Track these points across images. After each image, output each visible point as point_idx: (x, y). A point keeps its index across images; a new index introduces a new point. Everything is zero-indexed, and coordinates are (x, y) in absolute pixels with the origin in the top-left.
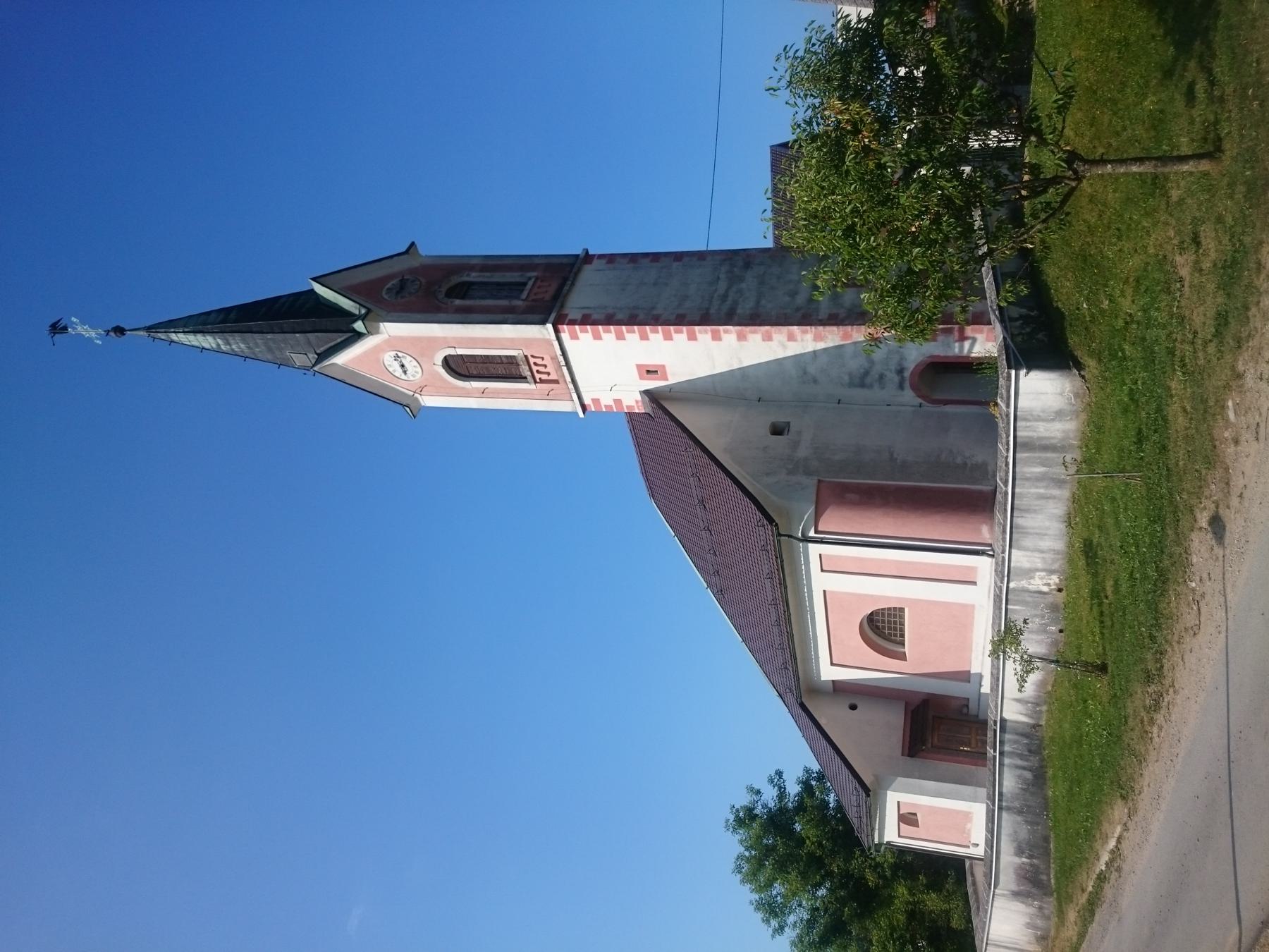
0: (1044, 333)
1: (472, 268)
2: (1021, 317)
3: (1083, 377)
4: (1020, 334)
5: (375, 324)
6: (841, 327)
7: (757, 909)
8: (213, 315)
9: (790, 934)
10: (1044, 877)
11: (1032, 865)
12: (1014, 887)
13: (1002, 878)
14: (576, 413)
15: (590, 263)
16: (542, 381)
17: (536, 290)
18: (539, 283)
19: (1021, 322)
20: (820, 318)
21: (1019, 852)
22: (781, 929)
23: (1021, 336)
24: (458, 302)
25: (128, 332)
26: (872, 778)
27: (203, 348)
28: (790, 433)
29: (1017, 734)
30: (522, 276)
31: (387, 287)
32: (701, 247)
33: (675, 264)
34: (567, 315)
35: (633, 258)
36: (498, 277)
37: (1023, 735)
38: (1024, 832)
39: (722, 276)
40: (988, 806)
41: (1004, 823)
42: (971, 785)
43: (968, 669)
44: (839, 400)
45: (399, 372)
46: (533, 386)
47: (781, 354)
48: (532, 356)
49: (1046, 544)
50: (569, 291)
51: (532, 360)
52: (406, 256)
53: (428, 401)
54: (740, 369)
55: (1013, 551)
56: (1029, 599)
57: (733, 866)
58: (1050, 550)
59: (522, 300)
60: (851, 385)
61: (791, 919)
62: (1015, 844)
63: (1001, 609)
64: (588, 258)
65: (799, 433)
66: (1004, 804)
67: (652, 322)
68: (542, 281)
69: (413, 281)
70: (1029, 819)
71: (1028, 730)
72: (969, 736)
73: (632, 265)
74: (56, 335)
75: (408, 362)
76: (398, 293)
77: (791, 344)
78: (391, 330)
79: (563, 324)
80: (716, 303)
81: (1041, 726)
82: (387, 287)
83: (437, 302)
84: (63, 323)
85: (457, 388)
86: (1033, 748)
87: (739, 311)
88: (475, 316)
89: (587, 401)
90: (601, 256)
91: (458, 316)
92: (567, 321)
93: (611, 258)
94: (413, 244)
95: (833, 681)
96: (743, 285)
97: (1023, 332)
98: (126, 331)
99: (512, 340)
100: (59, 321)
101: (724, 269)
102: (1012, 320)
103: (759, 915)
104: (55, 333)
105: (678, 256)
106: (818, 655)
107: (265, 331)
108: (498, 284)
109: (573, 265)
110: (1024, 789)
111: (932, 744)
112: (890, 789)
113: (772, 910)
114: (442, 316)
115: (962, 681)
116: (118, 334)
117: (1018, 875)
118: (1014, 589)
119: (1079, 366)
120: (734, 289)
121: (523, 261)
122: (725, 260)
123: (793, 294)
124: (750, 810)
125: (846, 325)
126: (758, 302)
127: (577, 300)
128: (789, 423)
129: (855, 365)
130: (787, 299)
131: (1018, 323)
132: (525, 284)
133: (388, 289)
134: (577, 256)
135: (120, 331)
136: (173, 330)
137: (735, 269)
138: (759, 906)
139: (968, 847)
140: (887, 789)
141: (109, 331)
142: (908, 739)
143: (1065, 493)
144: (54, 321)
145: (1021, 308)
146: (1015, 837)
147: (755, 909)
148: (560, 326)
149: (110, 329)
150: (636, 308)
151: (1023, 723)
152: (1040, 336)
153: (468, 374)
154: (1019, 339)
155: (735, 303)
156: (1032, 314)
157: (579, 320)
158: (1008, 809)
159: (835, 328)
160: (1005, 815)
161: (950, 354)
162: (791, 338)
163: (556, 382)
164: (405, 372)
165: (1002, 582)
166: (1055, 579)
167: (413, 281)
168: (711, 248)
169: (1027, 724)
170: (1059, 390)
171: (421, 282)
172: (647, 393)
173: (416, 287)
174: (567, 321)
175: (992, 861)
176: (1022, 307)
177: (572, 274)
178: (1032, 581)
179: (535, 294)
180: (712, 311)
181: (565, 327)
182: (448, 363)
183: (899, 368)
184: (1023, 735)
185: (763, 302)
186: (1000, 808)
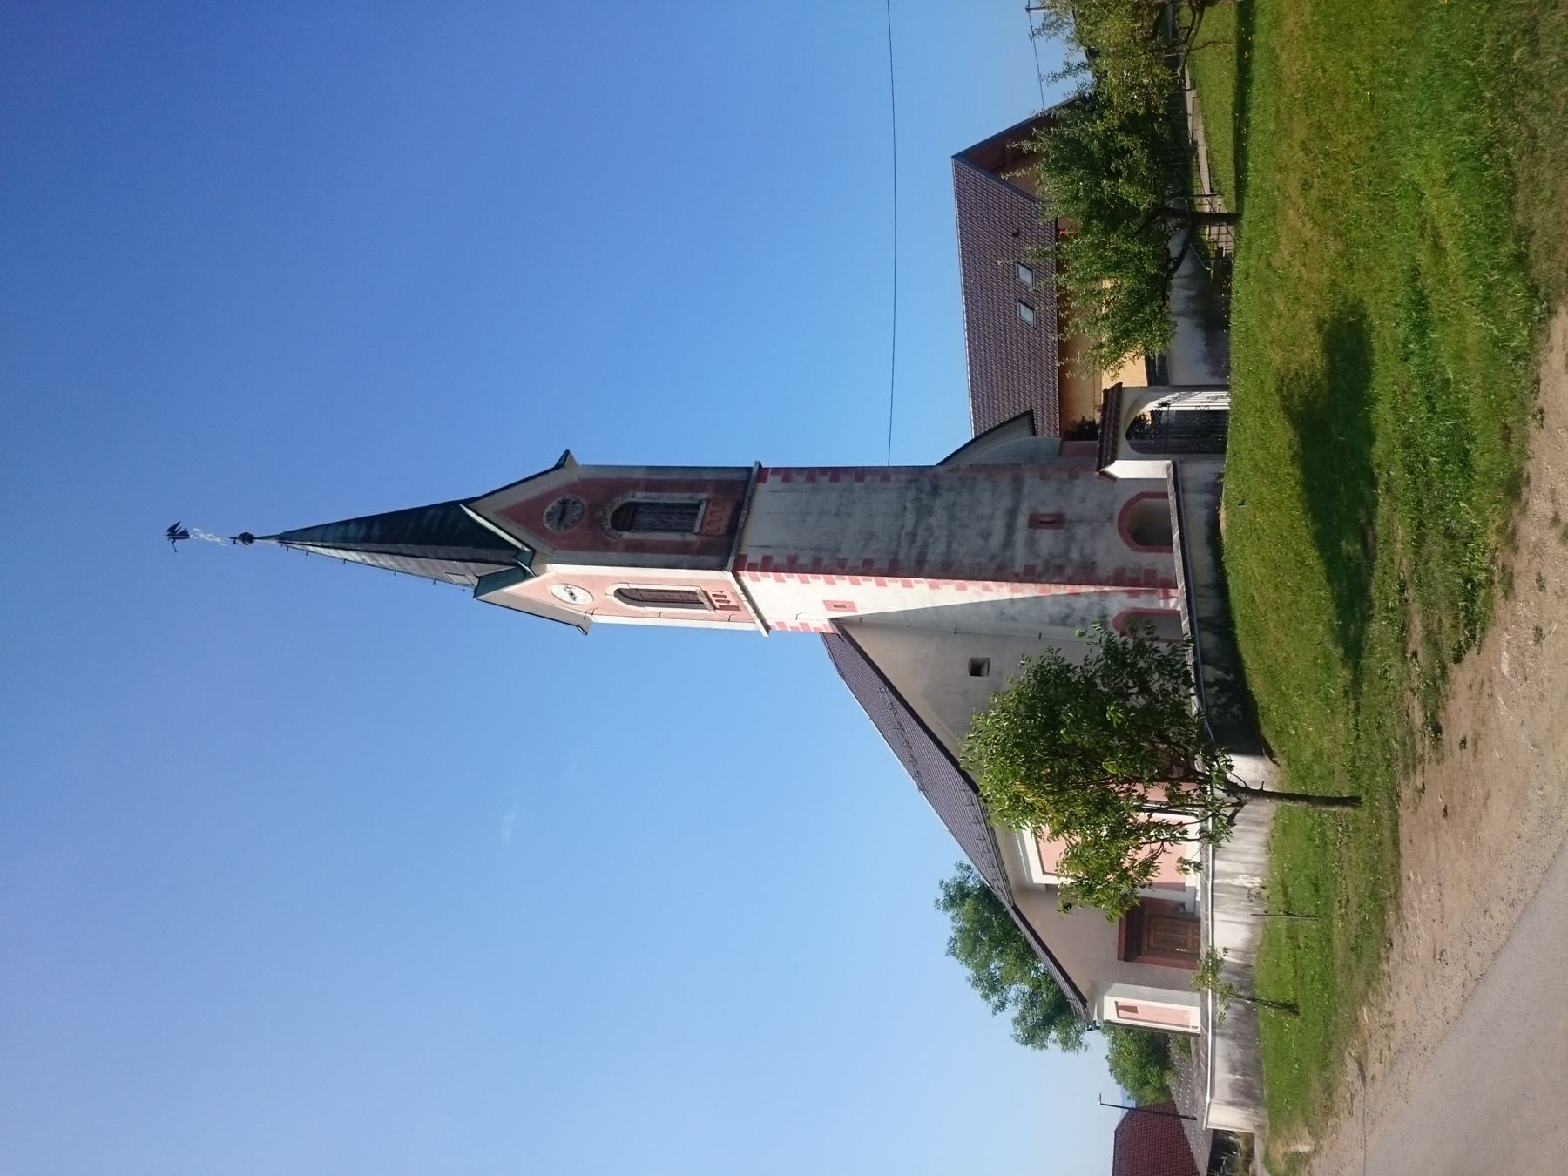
0: (1239, 705)
1: (634, 485)
2: (1218, 682)
3: (1275, 763)
4: (1215, 705)
5: (541, 566)
6: (1038, 585)
7: (975, 985)
8: (352, 527)
9: (1013, 1011)
10: (1258, 1092)
11: (1246, 1081)
12: (1229, 1099)
13: (1217, 1091)
14: (759, 632)
15: (764, 480)
16: (721, 608)
17: (709, 518)
18: (711, 508)
19: (1216, 688)
20: (1016, 571)
21: (1233, 1070)
22: (1001, 1006)
23: (1216, 709)
24: (627, 535)
25: (258, 541)
26: (1089, 985)
27: (345, 560)
28: (990, 672)
29: (1229, 972)
30: (691, 497)
31: (548, 510)
32: (881, 462)
33: (857, 485)
34: (746, 556)
35: (811, 474)
36: (666, 498)
37: (1234, 973)
38: (1237, 1054)
39: (909, 505)
40: (1202, 1009)
41: (1218, 1047)
42: (1187, 991)
43: (1182, 882)
44: (1040, 635)
45: (567, 598)
46: (713, 612)
47: (976, 600)
48: (714, 595)
49: (1249, 858)
50: (745, 523)
51: (710, 594)
52: (562, 470)
53: (597, 619)
54: (933, 608)
55: (1217, 862)
56: (1235, 891)
57: (946, 948)
58: (1252, 863)
59: (696, 534)
60: (1052, 622)
61: (1012, 993)
62: (1229, 1064)
63: (1207, 895)
64: (762, 473)
65: (1000, 673)
66: (1217, 1031)
67: (839, 570)
68: (714, 505)
69: (574, 503)
70: (1242, 1044)
71: (1239, 969)
72: (1185, 936)
73: (809, 485)
74: (177, 541)
75: (576, 591)
76: (560, 520)
77: (986, 593)
78: (554, 570)
79: (743, 570)
80: (905, 545)
81: (1252, 966)
82: (548, 510)
83: (604, 534)
84: (182, 528)
85: (631, 611)
86: (1244, 985)
87: (930, 557)
88: (647, 556)
89: (770, 623)
90: (776, 470)
91: (627, 556)
92: (746, 567)
93: (786, 474)
94: (567, 452)
95: (1046, 885)
96: (932, 520)
97: (1219, 702)
98: (255, 538)
99: (690, 580)
100: (177, 525)
101: (911, 494)
102: (1208, 685)
103: (978, 992)
104: (175, 539)
105: (860, 473)
106: (1028, 860)
107: (417, 554)
108: (667, 506)
109: (746, 483)
110: (1237, 1019)
111: (1148, 945)
112: (1110, 991)
113: (992, 986)
114: (613, 556)
115: (1177, 890)
116: (247, 542)
117: (1233, 1089)
118: (1219, 885)
119: (1271, 754)
120: (922, 525)
121: (690, 476)
122: (911, 482)
123: (986, 535)
124: (961, 887)
125: (1043, 583)
126: (949, 544)
127: (758, 532)
128: (988, 659)
129: (1055, 610)
130: (980, 542)
131: (1213, 690)
132: (697, 506)
133: (549, 514)
134: (749, 469)
135: (247, 538)
136: (309, 543)
137: (923, 496)
138: (976, 982)
139: (1188, 1027)
140: (1104, 993)
141: (235, 538)
142: (1123, 941)
143: (1265, 830)
144: (173, 524)
145: (1218, 670)
146: (1228, 1057)
147: (973, 986)
148: (740, 573)
149: (237, 536)
150: (819, 549)
151: (1234, 963)
152: (1235, 709)
153: (641, 599)
154: (1214, 712)
155: (925, 545)
156: (1228, 678)
157: (760, 564)
158: (1222, 1035)
159: (1032, 585)
160: (1218, 1040)
161: (1154, 607)
162: (986, 589)
163: (736, 608)
164: (574, 599)
165: (1207, 879)
166: (1258, 881)
167: (574, 503)
168: (893, 464)
169: (1239, 965)
170: (1253, 768)
171: (583, 506)
172: (834, 621)
173: (579, 511)
174: (746, 567)
175: (1207, 1078)
176: (1219, 668)
177: (747, 499)
178: (1236, 880)
179: (709, 523)
180: (901, 556)
181: (745, 572)
182: (620, 593)
183: (1101, 614)
184: (1234, 973)
185: (955, 546)
186: (1214, 1034)
